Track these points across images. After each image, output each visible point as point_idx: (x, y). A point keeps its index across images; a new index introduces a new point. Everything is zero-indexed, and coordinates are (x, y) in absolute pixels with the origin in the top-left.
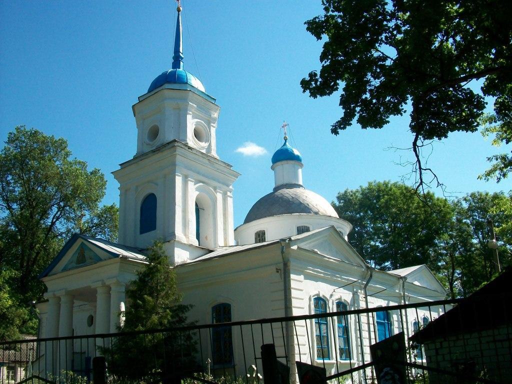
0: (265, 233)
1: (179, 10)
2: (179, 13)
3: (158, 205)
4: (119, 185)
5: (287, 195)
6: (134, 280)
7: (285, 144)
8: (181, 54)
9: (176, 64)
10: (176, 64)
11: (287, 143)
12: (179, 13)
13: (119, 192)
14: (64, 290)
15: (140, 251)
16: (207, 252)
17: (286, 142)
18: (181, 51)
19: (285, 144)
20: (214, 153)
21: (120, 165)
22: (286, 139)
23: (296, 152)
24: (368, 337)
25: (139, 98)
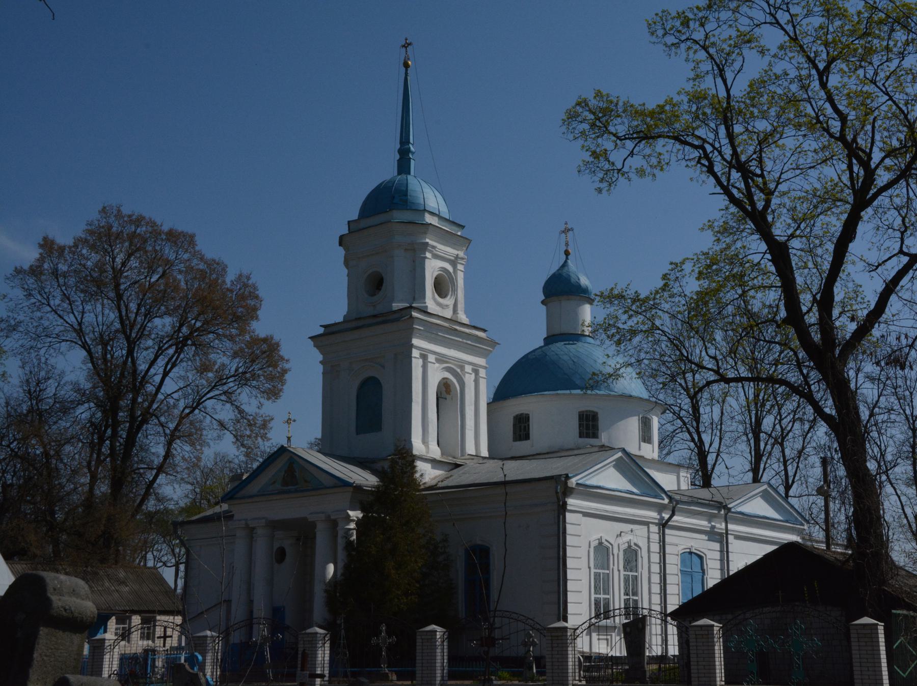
0: (529, 417)
1: (406, 66)
2: (406, 70)
3: (346, 290)
4: (320, 357)
5: (565, 358)
6: (275, 337)
7: (565, 264)
8: (411, 146)
9: (403, 166)
10: (403, 166)
11: (569, 261)
12: (406, 70)
13: (320, 368)
14: (264, 521)
15: (363, 463)
16: (454, 466)
17: (567, 258)
18: (411, 141)
19: (565, 264)
20: (463, 317)
21: (325, 326)
22: (567, 253)
23: (584, 281)
24: (652, 555)
25: (349, 222)
